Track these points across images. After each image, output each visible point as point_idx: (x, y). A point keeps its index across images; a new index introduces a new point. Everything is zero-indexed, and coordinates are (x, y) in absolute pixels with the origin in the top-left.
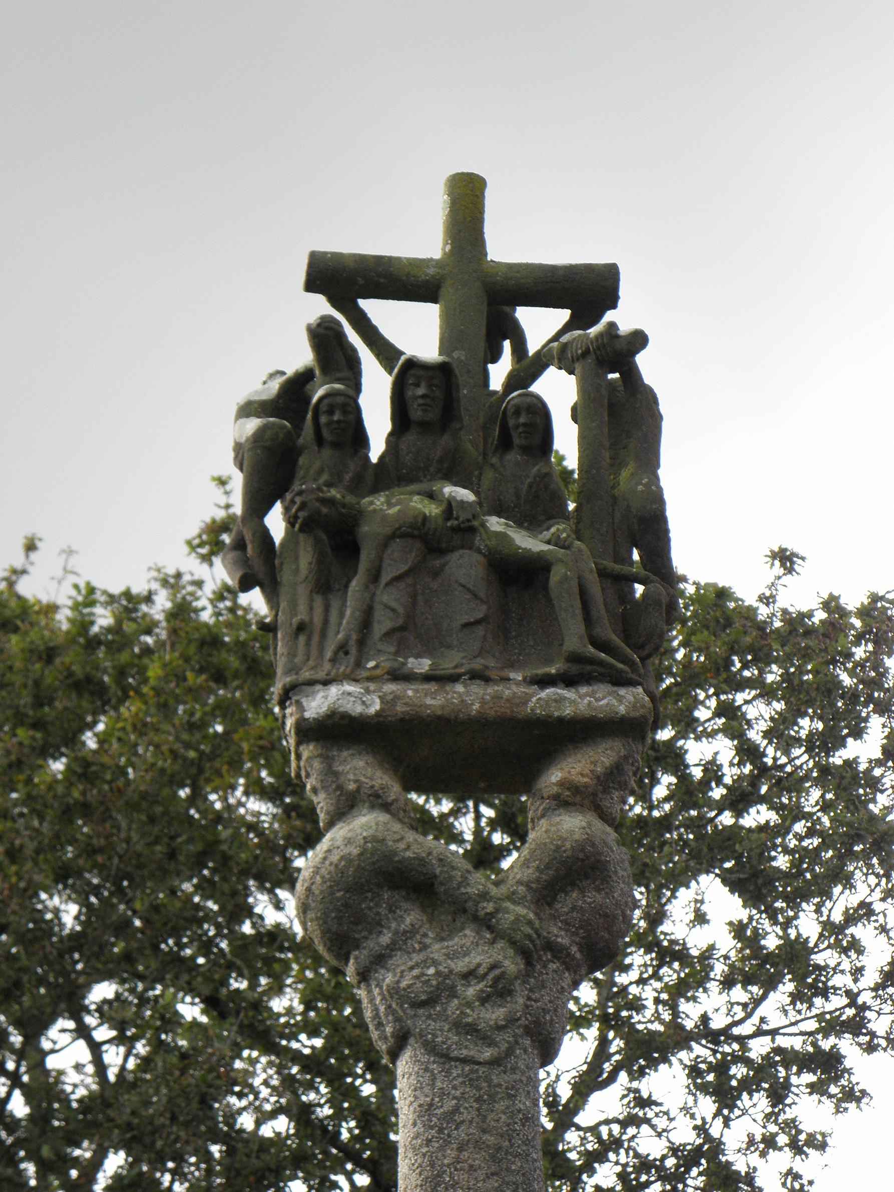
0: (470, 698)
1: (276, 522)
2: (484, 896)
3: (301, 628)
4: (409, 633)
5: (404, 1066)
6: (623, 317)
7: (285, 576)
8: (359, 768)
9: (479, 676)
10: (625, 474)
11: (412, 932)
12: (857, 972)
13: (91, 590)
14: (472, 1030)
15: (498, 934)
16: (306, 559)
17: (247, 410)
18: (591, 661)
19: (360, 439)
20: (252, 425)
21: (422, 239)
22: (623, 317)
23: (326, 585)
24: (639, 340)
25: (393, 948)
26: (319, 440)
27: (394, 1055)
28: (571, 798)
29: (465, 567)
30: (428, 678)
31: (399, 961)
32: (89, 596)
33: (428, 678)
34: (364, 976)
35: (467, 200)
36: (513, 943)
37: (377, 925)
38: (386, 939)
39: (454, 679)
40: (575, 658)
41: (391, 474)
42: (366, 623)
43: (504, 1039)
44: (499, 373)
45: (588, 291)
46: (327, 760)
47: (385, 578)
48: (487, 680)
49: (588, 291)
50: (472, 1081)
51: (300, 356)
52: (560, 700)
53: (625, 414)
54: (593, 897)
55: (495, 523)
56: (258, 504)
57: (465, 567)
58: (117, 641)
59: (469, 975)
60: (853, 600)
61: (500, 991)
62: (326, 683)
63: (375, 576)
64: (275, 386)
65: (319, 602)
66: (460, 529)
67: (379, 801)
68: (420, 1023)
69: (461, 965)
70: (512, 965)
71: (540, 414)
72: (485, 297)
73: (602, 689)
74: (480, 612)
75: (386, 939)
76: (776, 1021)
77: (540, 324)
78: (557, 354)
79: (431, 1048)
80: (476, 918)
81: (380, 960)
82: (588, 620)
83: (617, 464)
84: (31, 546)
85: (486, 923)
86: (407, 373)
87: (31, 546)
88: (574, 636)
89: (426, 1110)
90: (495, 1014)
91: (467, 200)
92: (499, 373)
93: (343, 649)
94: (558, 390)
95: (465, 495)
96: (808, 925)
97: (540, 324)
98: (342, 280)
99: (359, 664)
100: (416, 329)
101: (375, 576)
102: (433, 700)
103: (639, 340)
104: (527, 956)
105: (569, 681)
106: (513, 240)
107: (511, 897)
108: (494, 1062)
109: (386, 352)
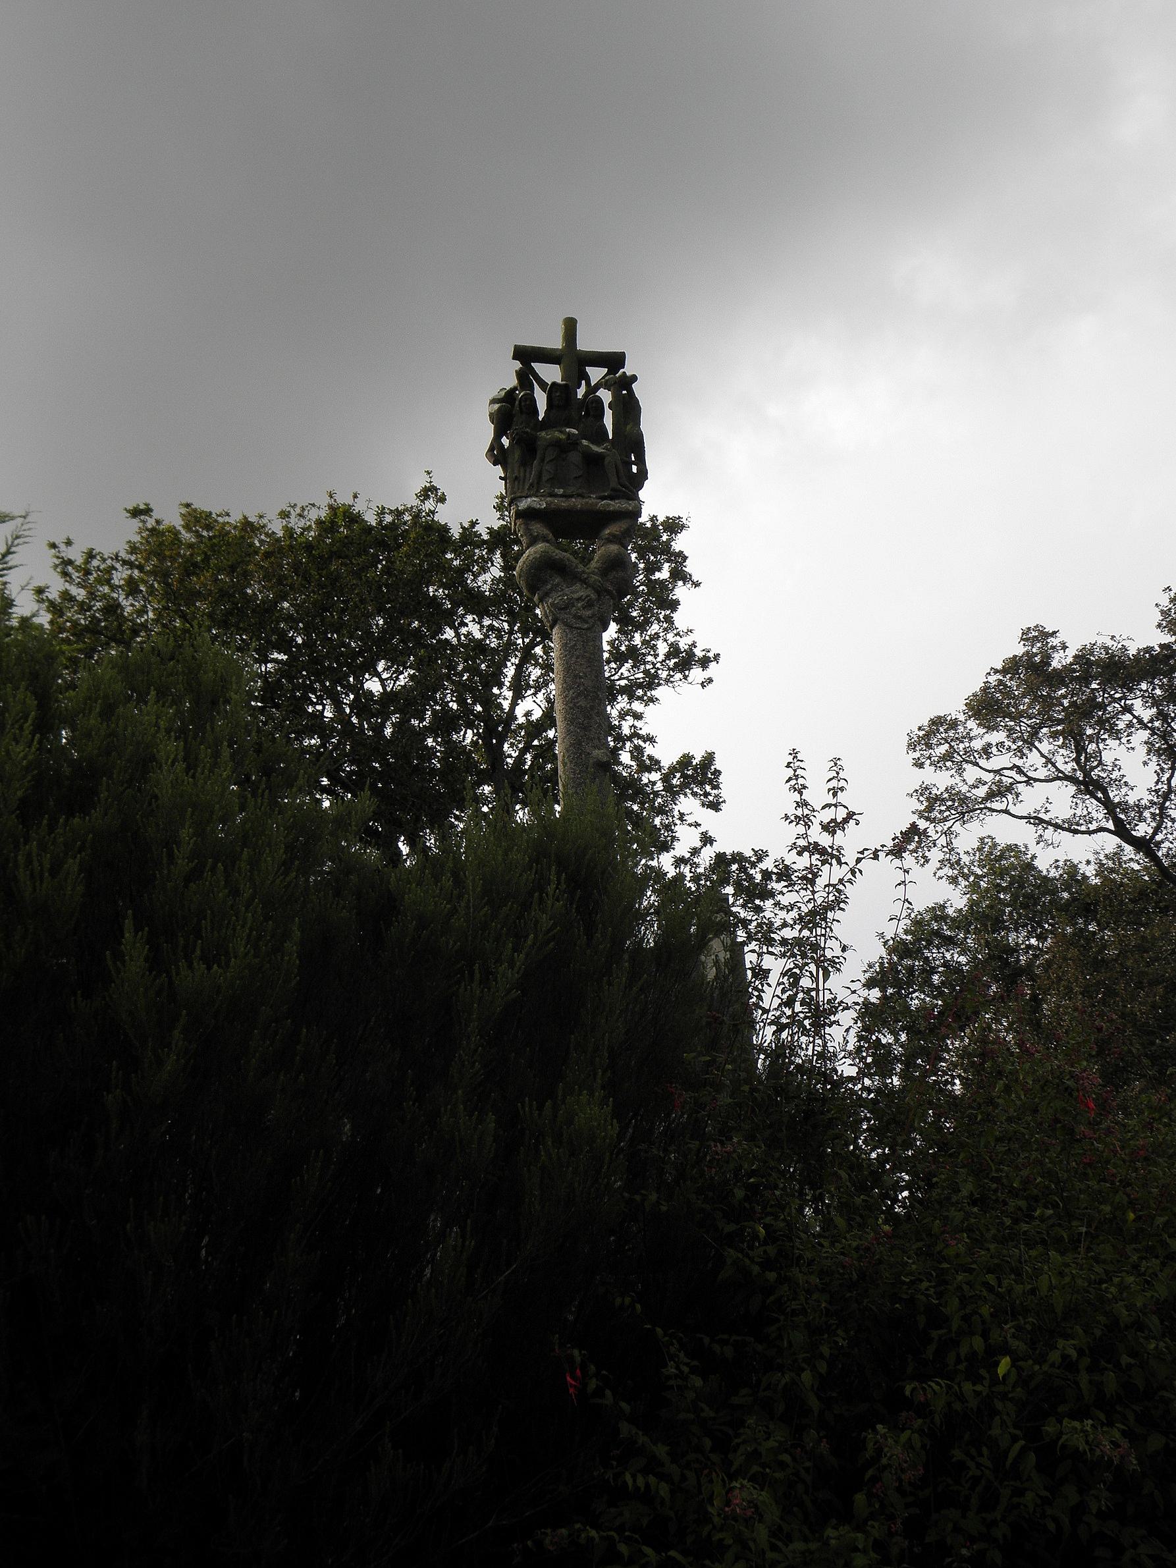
0: (577, 503)
1: (505, 441)
2: (583, 572)
3: (516, 478)
4: (555, 481)
5: (556, 633)
6: (628, 370)
7: (510, 460)
8: (538, 528)
9: (581, 496)
10: (629, 427)
11: (558, 585)
12: (656, 656)
13: (384, 508)
14: (580, 618)
15: (588, 585)
16: (517, 454)
17: (493, 401)
18: (620, 491)
19: (536, 412)
20: (496, 406)
21: (555, 342)
22: (628, 370)
23: (525, 463)
24: (634, 378)
25: (551, 590)
26: (521, 412)
27: (552, 628)
28: (612, 539)
29: (574, 457)
30: (562, 496)
31: (554, 594)
32: (381, 512)
33: (562, 496)
34: (541, 600)
35: (570, 326)
36: (594, 588)
37: (545, 582)
38: (549, 587)
39: (572, 496)
40: (613, 490)
41: (547, 424)
42: (540, 476)
43: (591, 621)
44: (581, 392)
45: (614, 361)
46: (526, 524)
47: (547, 459)
48: (583, 497)
49: (614, 361)
50: (580, 635)
51: (513, 382)
52: (609, 505)
53: (628, 409)
54: (621, 574)
55: (585, 442)
56: (498, 435)
57: (574, 457)
58: (392, 526)
59: (579, 599)
60: (661, 519)
61: (589, 605)
62: (526, 497)
63: (543, 460)
64: (503, 393)
65: (522, 470)
66: (573, 443)
67: (545, 539)
68: (562, 616)
69: (575, 596)
70: (593, 596)
71: (599, 402)
72: (575, 361)
73: (623, 501)
74: (580, 473)
75: (549, 587)
76: (626, 674)
77: (596, 374)
78: (604, 384)
79: (566, 624)
80: (580, 580)
81: (547, 594)
82: (619, 478)
83: (626, 424)
84: (355, 497)
85: (584, 582)
86: (552, 390)
87: (355, 497)
88: (614, 483)
89: (564, 646)
90: (589, 613)
91: (570, 326)
92: (581, 392)
93: (532, 485)
94: (606, 396)
95: (575, 431)
96: (637, 639)
97: (596, 374)
98: (526, 356)
99: (538, 491)
100: (551, 373)
101: (543, 460)
102: (564, 504)
103: (634, 378)
104: (599, 593)
105: (612, 498)
106: (586, 343)
107: (593, 573)
108: (587, 629)
109: (543, 384)
